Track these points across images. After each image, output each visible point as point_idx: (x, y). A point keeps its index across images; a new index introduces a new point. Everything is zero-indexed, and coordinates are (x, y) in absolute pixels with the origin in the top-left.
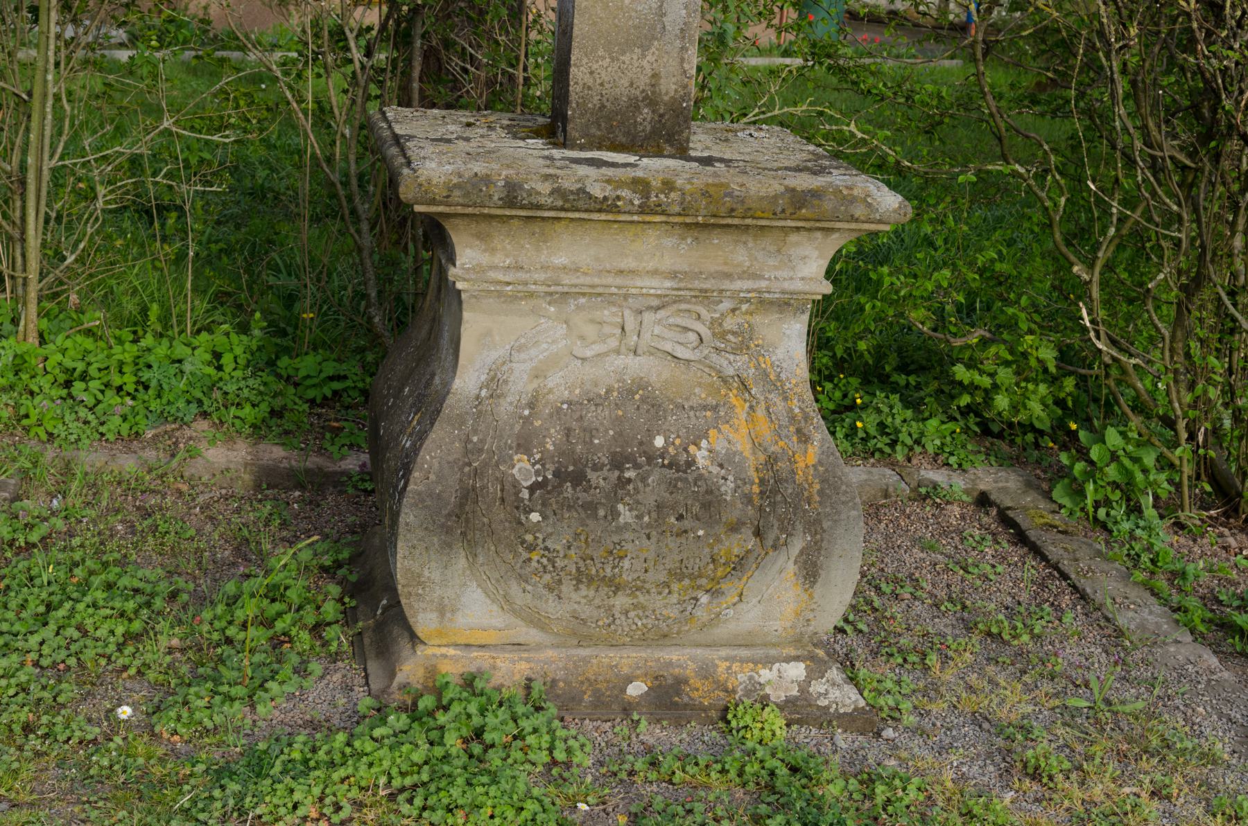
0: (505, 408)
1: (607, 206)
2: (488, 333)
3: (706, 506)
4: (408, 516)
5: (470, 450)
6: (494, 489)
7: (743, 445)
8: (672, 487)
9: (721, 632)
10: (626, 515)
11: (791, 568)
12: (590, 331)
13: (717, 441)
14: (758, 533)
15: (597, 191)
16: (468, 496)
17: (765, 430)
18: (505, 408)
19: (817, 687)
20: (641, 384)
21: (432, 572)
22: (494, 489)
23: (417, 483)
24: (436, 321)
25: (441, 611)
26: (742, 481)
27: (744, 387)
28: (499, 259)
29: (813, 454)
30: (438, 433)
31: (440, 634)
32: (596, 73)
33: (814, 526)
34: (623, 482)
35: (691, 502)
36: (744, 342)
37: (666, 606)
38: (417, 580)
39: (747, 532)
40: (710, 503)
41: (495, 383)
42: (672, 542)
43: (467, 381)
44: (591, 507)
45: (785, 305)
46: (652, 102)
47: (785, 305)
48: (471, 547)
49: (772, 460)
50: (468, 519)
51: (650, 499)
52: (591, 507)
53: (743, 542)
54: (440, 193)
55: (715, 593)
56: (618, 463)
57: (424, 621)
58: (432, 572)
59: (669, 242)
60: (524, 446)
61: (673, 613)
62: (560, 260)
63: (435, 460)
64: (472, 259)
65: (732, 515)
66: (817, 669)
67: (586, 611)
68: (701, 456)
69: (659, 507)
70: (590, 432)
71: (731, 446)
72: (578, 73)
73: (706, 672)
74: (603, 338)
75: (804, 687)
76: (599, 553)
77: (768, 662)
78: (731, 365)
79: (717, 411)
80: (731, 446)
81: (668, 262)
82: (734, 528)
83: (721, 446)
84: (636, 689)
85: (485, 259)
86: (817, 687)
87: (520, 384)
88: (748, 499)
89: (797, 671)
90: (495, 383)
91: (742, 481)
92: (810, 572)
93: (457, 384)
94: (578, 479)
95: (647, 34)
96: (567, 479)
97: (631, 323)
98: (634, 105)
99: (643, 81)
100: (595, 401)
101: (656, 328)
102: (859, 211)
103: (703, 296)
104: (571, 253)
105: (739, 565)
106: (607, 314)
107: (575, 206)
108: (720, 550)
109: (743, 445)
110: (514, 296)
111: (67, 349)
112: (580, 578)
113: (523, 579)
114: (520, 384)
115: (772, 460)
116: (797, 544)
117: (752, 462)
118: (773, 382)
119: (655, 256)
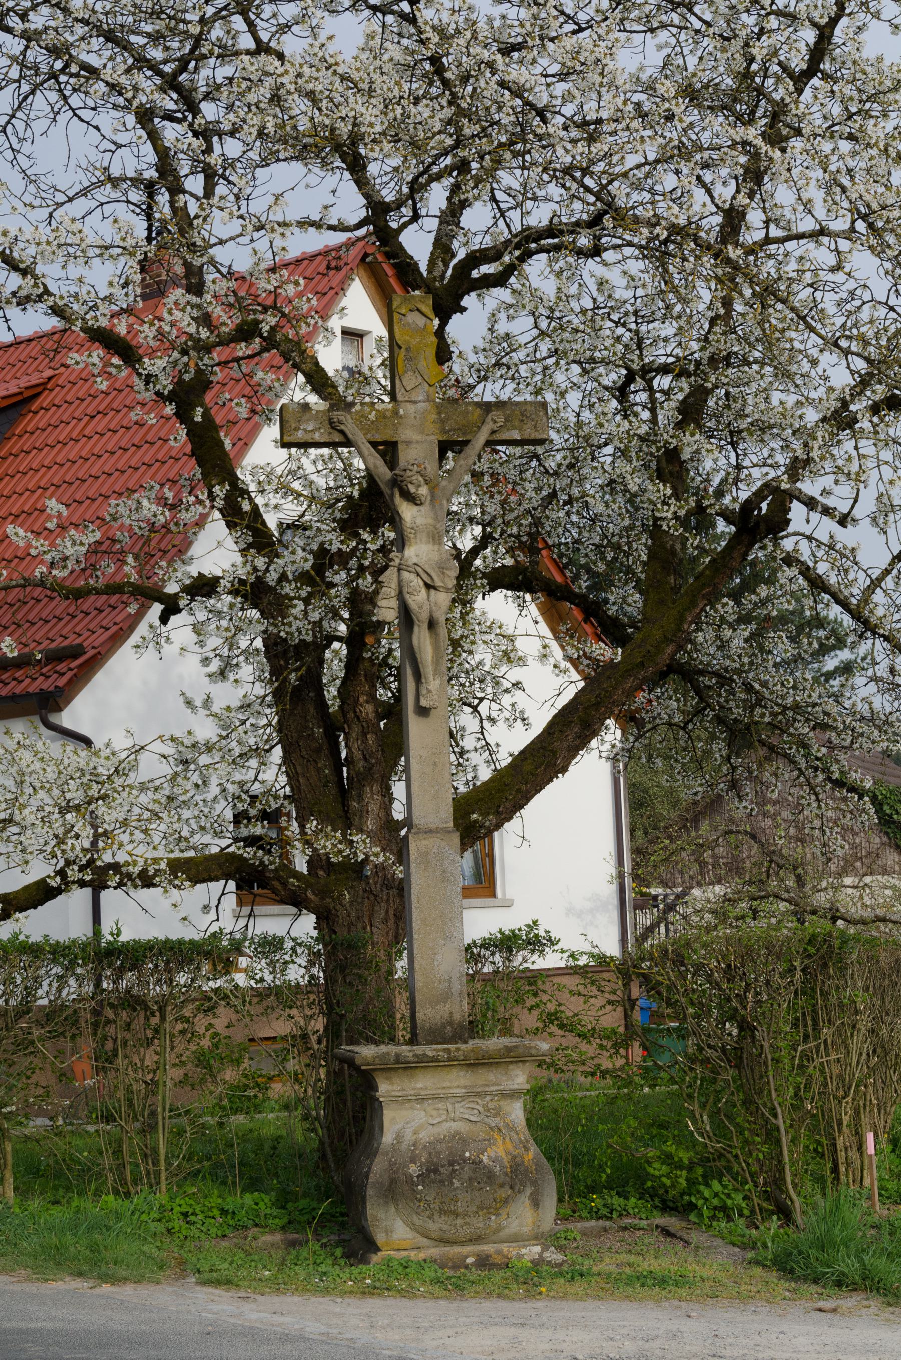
0: (404, 1146)
1: (435, 1059)
2: (394, 1118)
3: (489, 1178)
4: (370, 1192)
5: (391, 1164)
6: (403, 1178)
7: (501, 1153)
8: (474, 1171)
9: (503, 1234)
10: (457, 1184)
11: (527, 1202)
12: (435, 1113)
13: (491, 1152)
14: (511, 1188)
15: (430, 1054)
16: (393, 1181)
17: (510, 1146)
18: (404, 1146)
19: (546, 1255)
20: (457, 1133)
21: (382, 1215)
22: (403, 1178)
23: (372, 1179)
24: (372, 1129)
25: (387, 1232)
26: (502, 1167)
27: (499, 1130)
28: (395, 1087)
29: (531, 1155)
30: (378, 1159)
31: (387, 1244)
32: (427, 1014)
33: (534, 1183)
34: (454, 1171)
35: (483, 1176)
36: (497, 1113)
37: (478, 1224)
38: (376, 1219)
39: (507, 1187)
40: (490, 1176)
41: (399, 1138)
42: (477, 1193)
43: (388, 1138)
44: (442, 1182)
45: (513, 1095)
46: (451, 1023)
47: (513, 1095)
48: (396, 1202)
49: (514, 1158)
50: (396, 1190)
51: (466, 1177)
52: (442, 1182)
53: (505, 1192)
54: (370, 1060)
55: (497, 1215)
56: (451, 1164)
57: (380, 1238)
58: (382, 1215)
59: (461, 1074)
60: (413, 1161)
61: (481, 1225)
62: (420, 1085)
63: (378, 1168)
64: (385, 1088)
65: (501, 1180)
66: (545, 1248)
67: (445, 1227)
68: (485, 1159)
69: (470, 1179)
70: (439, 1153)
71: (496, 1154)
72: (420, 1015)
73: (499, 1252)
74: (440, 1115)
75: (540, 1255)
76: (447, 1200)
77: (525, 1247)
78: (493, 1122)
79: (490, 1142)
80: (496, 1154)
81: (463, 1082)
82: (501, 1186)
83: (492, 1155)
84: (470, 1260)
85: (390, 1088)
86: (546, 1255)
87: (409, 1137)
88: (506, 1174)
89: (537, 1249)
90: (399, 1138)
91: (502, 1167)
92: (536, 1203)
93: (384, 1140)
94: (436, 1171)
95: (445, 997)
96: (431, 1171)
97: (450, 1108)
98: (444, 1026)
99: (446, 1016)
100: (440, 1141)
101: (461, 1110)
102: (533, 1052)
103: (478, 1094)
104: (424, 1082)
105: (506, 1201)
106: (440, 1106)
107: (423, 1064)
108: (497, 1195)
109: (501, 1153)
110: (403, 1101)
111: (182, 1204)
112: (442, 1212)
113: (418, 1214)
114: (409, 1137)
115: (514, 1158)
116: (529, 1191)
117: (506, 1159)
118: (512, 1129)
119: (456, 1081)
